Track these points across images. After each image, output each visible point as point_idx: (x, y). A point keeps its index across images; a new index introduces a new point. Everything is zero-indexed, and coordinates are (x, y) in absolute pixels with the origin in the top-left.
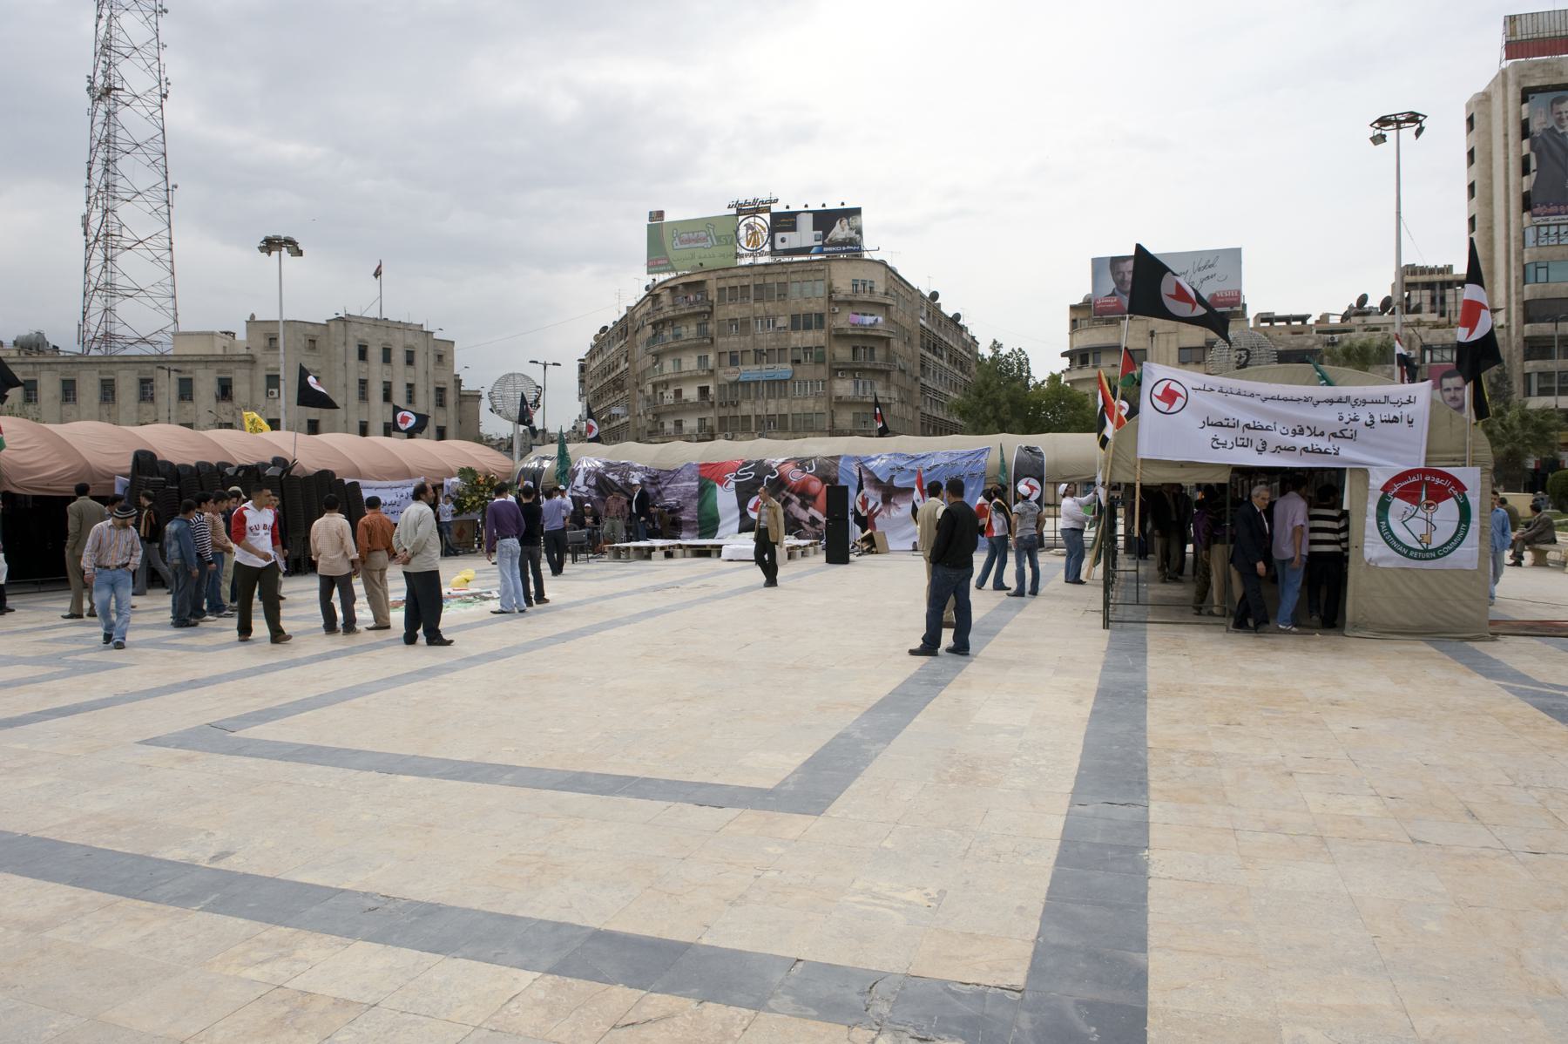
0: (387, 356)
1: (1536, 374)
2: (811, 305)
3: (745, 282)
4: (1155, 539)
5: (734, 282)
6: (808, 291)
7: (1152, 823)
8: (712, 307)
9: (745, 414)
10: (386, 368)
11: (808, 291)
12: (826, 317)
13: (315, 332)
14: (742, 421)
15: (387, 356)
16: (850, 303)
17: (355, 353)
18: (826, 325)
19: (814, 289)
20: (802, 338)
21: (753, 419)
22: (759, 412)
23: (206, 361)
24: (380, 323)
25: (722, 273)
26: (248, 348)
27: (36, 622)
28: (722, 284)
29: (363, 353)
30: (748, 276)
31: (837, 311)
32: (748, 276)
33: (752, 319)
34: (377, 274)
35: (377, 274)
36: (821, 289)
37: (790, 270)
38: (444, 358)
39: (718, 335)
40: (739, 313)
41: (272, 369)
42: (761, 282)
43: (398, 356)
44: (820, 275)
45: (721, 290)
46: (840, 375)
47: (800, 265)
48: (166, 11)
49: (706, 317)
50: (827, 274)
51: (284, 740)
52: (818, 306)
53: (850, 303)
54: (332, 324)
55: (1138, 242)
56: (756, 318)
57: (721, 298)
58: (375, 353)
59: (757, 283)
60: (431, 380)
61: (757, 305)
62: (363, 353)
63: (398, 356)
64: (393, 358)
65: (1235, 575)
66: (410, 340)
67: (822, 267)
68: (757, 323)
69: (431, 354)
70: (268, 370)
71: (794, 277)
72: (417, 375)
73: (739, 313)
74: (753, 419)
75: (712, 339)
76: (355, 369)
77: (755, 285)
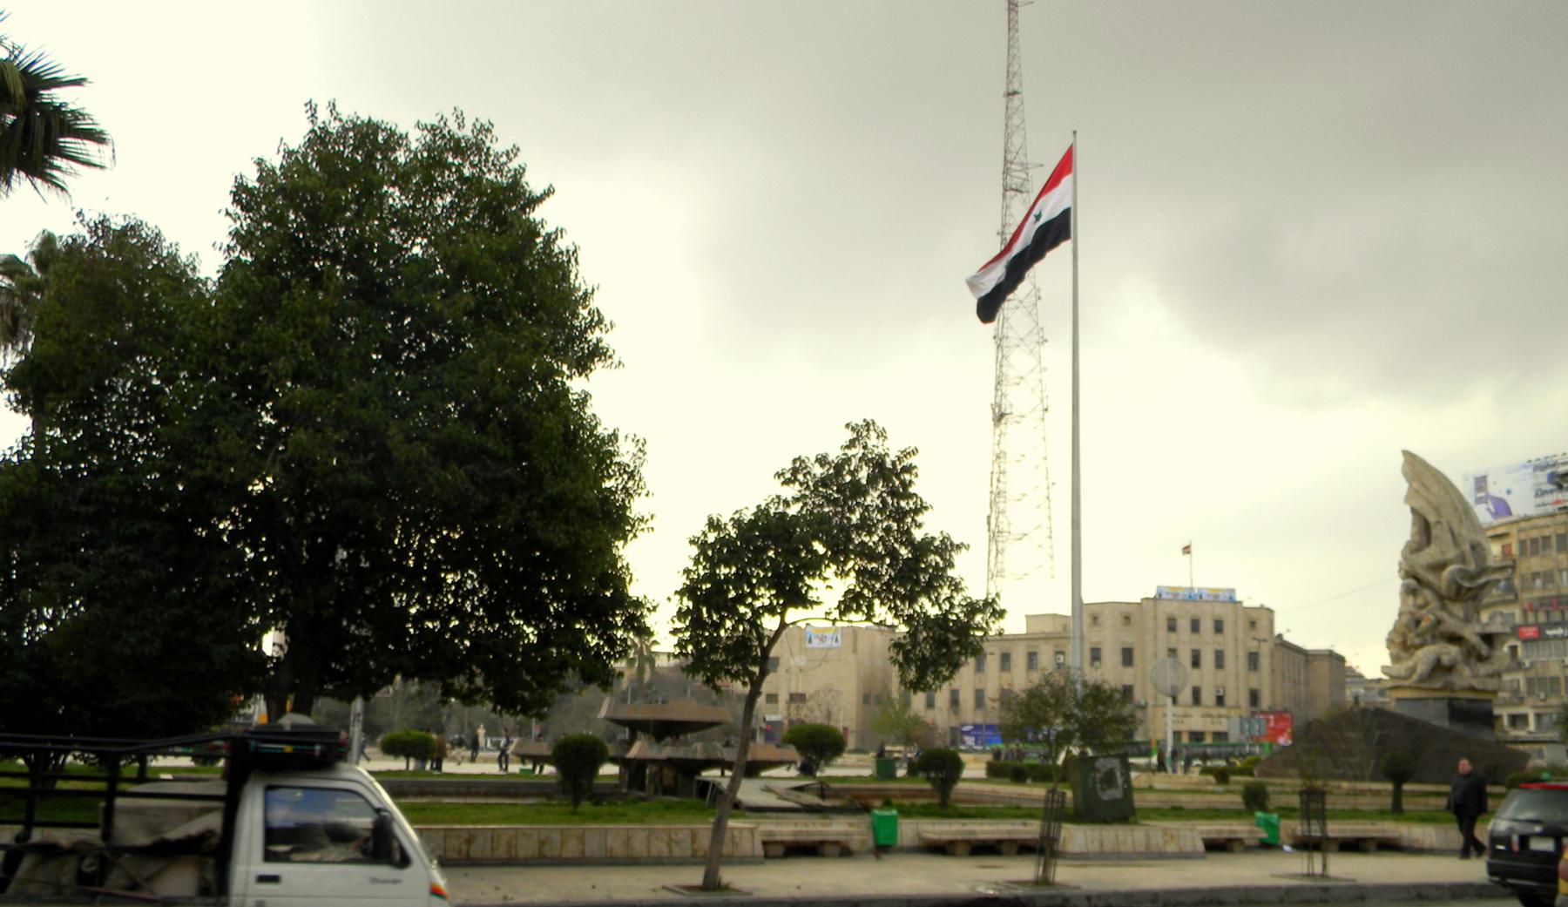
0: (1195, 626)
3: (1547, 532)
4: (18, 829)
5: (1534, 534)
7: (1102, 844)
15: (1195, 626)
22: (1501, 695)
23: (1047, 638)
25: (1523, 525)
27: (984, 849)
28: (1523, 536)
29: (1172, 627)
30: (1548, 526)
32: (1548, 526)
33: (1556, 572)
43: (1207, 626)
45: (1522, 543)
51: (1071, 869)
58: (1184, 625)
62: (1172, 627)
63: (1207, 626)
69: (1240, 621)
72: (1227, 641)
75: (1516, 596)
76: (1165, 639)
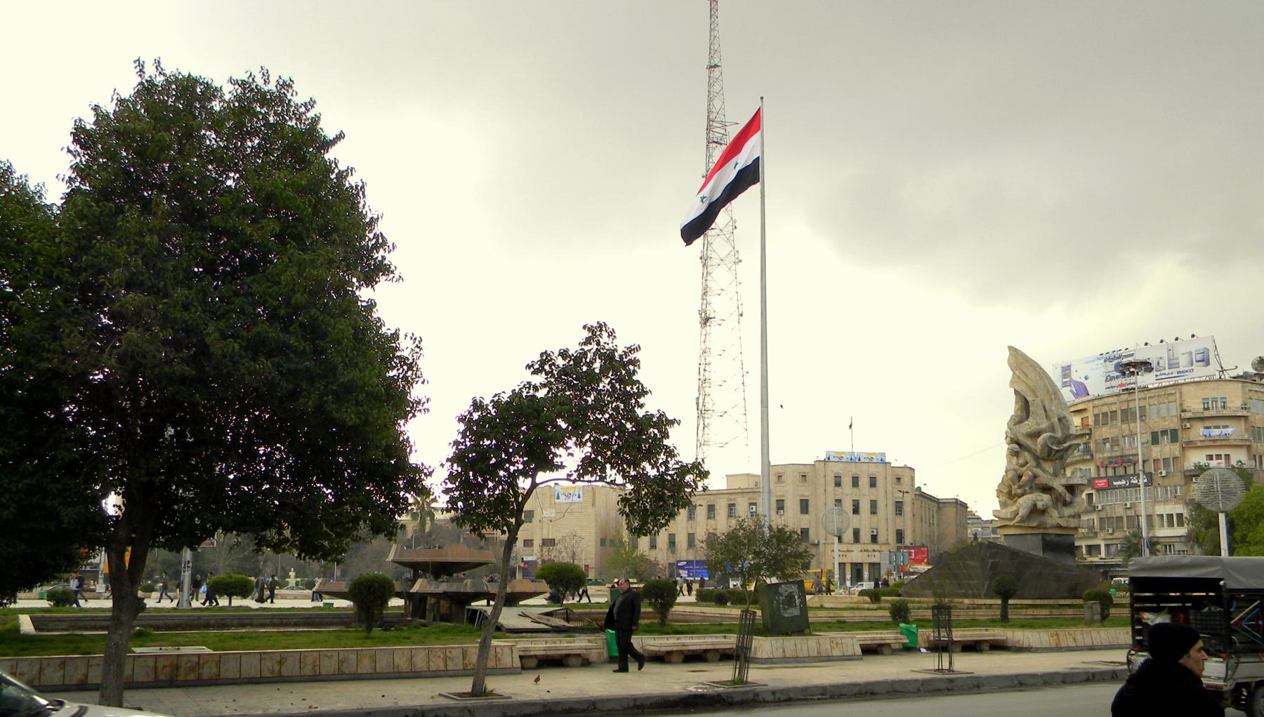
0: (855, 482)
1: (867, 565)
2: (1167, 423)
5: (1105, 409)
6: (1164, 413)
8: (1091, 430)
9: (1118, 515)
10: (855, 490)
11: (1164, 413)
12: (1179, 433)
13: (806, 470)
14: (1117, 521)
15: (855, 482)
16: (1202, 419)
17: (831, 482)
18: (1180, 438)
19: (1168, 410)
20: (1161, 451)
21: (1125, 519)
23: (743, 492)
24: (855, 460)
26: (1086, 378)
28: (1097, 411)
31: (1188, 425)
32: (1115, 403)
33: (1120, 438)
34: (850, 426)
35: (850, 426)
36: (1174, 411)
37: (1148, 396)
38: (902, 481)
39: (1096, 451)
40: (1110, 433)
41: (780, 496)
42: (1126, 407)
43: (864, 482)
44: (1172, 398)
45: (1096, 416)
46: (1194, 481)
47: (1157, 390)
48: (741, 261)
49: (1087, 437)
50: (1178, 397)
52: (1173, 424)
53: (1202, 419)
54: (817, 463)
55: (799, 513)
56: (1124, 437)
57: (1096, 422)
58: (846, 481)
59: (1123, 408)
60: (889, 496)
61: (1123, 426)
63: (864, 482)
64: (860, 483)
65: (521, 603)
66: (873, 470)
67: (1173, 392)
68: (1124, 440)
70: (777, 496)
71: (1152, 401)
72: (879, 494)
73: (1110, 433)
74: (1125, 519)
75: (1092, 456)
77: (1121, 410)
